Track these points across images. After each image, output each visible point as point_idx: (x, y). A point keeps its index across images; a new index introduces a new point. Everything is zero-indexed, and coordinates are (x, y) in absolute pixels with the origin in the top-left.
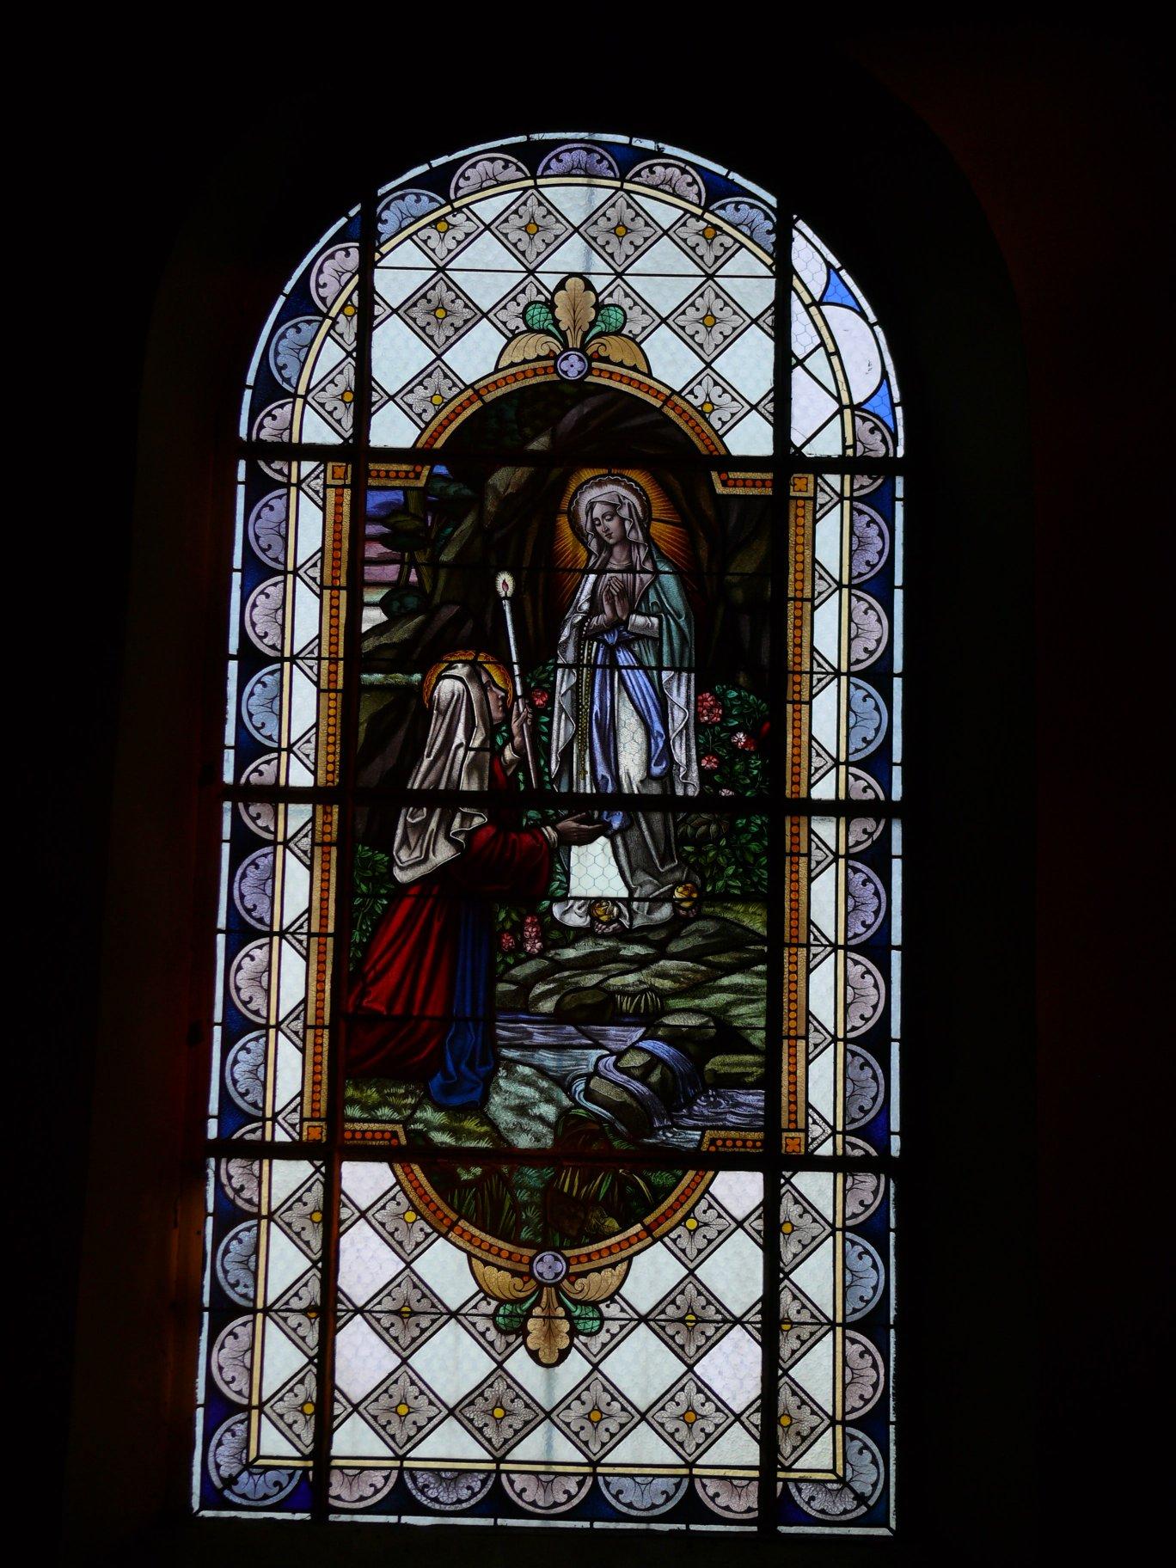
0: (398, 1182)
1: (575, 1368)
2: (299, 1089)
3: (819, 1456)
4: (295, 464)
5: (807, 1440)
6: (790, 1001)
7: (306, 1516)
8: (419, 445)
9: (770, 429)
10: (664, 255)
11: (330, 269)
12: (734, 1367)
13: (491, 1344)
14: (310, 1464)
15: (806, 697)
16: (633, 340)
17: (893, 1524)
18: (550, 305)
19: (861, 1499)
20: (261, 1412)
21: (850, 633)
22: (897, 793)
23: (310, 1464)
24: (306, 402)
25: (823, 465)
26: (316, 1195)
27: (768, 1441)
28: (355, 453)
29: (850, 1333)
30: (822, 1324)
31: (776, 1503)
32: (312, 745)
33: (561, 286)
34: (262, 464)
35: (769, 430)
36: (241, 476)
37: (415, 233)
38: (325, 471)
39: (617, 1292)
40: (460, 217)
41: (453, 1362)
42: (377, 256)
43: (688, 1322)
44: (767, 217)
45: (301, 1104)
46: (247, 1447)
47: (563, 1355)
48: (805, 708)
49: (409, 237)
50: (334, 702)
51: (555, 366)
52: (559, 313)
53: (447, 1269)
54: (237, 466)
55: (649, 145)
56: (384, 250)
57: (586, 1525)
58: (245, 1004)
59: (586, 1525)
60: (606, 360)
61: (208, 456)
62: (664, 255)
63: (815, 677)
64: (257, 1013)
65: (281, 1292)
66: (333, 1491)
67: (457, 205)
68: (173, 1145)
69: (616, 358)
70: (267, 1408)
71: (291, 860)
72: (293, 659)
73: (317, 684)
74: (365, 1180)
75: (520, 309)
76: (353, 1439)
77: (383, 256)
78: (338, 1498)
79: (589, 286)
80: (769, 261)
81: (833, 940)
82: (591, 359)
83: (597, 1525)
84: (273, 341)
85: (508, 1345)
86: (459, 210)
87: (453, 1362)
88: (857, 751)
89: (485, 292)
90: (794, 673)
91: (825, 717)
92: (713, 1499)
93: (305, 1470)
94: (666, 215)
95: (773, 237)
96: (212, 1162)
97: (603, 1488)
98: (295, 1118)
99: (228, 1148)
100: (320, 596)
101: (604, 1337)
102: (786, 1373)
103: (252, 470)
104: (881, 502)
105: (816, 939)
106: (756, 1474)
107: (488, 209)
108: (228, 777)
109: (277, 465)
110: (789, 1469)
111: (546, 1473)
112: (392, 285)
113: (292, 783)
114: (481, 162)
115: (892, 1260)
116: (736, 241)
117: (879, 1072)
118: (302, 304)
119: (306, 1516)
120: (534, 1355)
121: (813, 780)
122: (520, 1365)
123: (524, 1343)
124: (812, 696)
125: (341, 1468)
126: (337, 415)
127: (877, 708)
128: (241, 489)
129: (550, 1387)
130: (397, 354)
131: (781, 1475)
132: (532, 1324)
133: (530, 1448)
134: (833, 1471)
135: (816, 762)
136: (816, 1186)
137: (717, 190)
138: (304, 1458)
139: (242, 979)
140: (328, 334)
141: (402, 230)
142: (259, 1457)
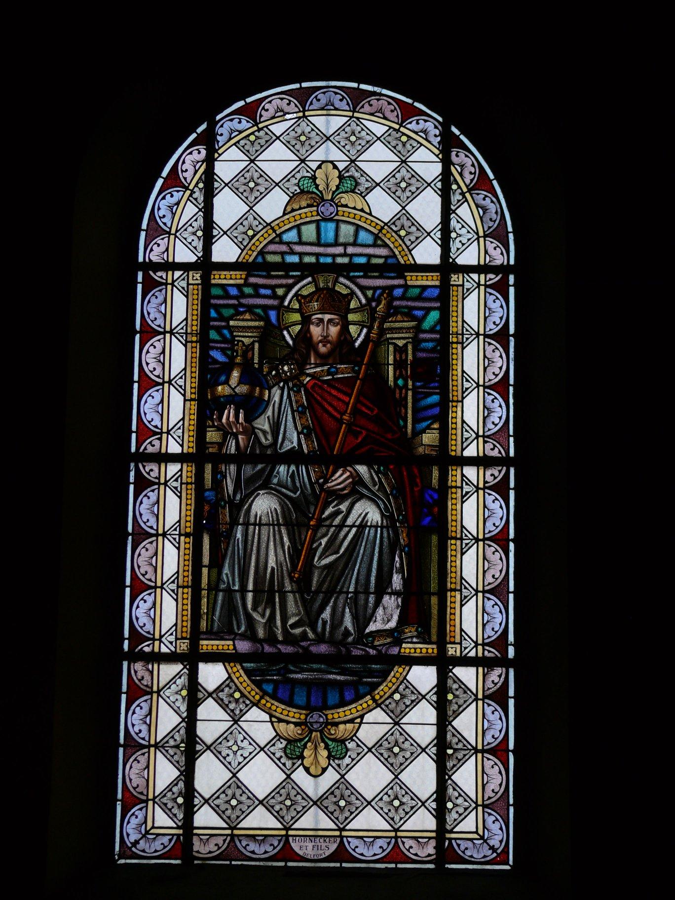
0: (410, 251)
1: (331, 777)
2: (183, 367)
3: (469, 824)
4: (480, 655)
5: (462, 817)
6: (451, 614)
7: (178, 862)
8: (240, 260)
9: (440, 199)
10: (379, 151)
11: (188, 159)
12: (421, 776)
13: (284, 764)
14: (181, 832)
15: (460, 399)
16: (361, 195)
17: (511, 863)
18: (314, 178)
19: (492, 848)
20: (159, 695)
21: (486, 312)
22: (512, 453)
23: (181, 832)
24: (176, 237)
25: (467, 269)
26: (454, 246)
27: (440, 814)
28: (205, 265)
29: (489, 290)
30: (472, 335)
31: (445, 851)
32: (181, 431)
33: (319, 167)
34: (151, 273)
35: (438, 250)
36: (140, 279)
37: (238, 142)
38: (188, 275)
39: (355, 735)
40: (262, 133)
41: (262, 775)
42: (216, 155)
43: (394, 752)
44: (436, 127)
45: (177, 578)
46: (145, 822)
47: (324, 770)
48: (460, 404)
49: (235, 144)
50: (194, 406)
51: (317, 211)
52: (318, 182)
53: (259, 725)
54: (122, 665)
55: (369, 88)
56: (220, 151)
57: (338, 865)
58: (149, 422)
59: (338, 865)
60: (346, 206)
61: (123, 275)
62: (379, 151)
63: (464, 542)
64: (151, 527)
65: (168, 680)
66: (195, 848)
67: (260, 126)
68: (104, 659)
69: (351, 205)
70: (163, 639)
71: (169, 492)
72: (164, 535)
73: (184, 395)
74: (212, 675)
75: (297, 181)
76: (205, 817)
77: (220, 155)
78: (198, 852)
79: (335, 167)
80: (437, 152)
81: (475, 535)
82: (337, 206)
83: (344, 865)
84: (160, 203)
85: (294, 764)
86: (262, 129)
87: (262, 775)
88: (489, 584)
89: (277, 172)
90: (452, 487)
91: (470, 410)
92: (418, 120)
93: (178, 835)
94: (379, 129)
95: (439, 139)
96: (512, 262)
97: (346, 844)
98: (172, 638)
99: (135, 656)
100: (185, 346)
101: (298, 176)
102: (450, 778)
103: (146, 277)
104: (501, 288)
105: (466, 536)
106: (434, 834)
107: (278, 129)
108: (133, 449)
109: (159, 274)
110: (451, 832)
111: (315, 835)
112: (225, 170)
113: (169, 451)
114: (273, 98)
115: (511, 401)
116: (418, 142)
117: (502, 714)
118: (174, 180)
119: (178, 862)
120: (307, 770)
121: (465, 445)
122: (300, 776)
123: (340, 172)
124: (463, 398)
125: (198, 835)
126: (194, 244)
127: (502, 307)
128: (132, 487)
129: (328, 149)
130: (228, 208)
131: (448, 836)
132: (306, 753)
133: (337, 122)
134: (476, 832)
135: (466, 435)
136: (184, 255)
137: (407, 113)
138: (178, 828)
139: (144, 508)
140: (188, 199)
141: (230, 139)
142: (153, 827)
